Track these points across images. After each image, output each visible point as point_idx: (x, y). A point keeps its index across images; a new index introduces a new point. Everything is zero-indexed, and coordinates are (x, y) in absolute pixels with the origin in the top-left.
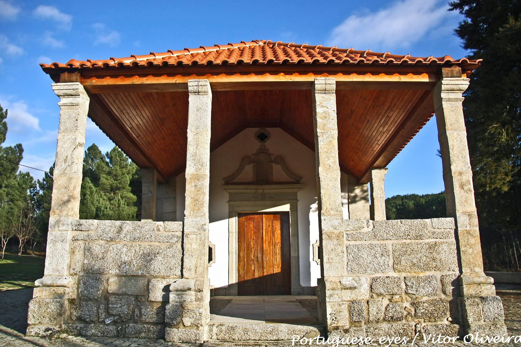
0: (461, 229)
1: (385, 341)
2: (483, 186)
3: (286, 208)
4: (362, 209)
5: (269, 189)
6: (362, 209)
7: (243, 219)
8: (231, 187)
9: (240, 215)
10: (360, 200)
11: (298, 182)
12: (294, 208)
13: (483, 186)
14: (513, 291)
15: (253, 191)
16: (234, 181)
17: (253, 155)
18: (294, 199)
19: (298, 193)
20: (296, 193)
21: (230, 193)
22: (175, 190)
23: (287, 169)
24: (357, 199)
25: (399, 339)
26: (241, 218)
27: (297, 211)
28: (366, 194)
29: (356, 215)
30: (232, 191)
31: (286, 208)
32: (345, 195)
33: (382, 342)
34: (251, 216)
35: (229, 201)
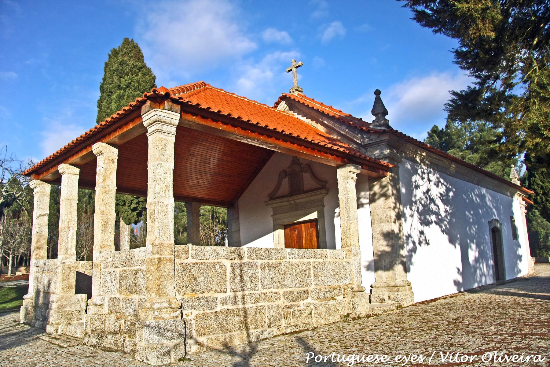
0: (168, 164)
1: (401, 359)
2: (144, 75)
3: (314, 215)
4: (383, 206)
5: (301, 199)
6: (383, 206)
7: (288, 230)
8: (273, 202)
9: (285, 227)
10: (379, 198)
11: (323, 187)
12: (321, 214)
13: (144, 75)
14: (523, 292)
15: (287, 203)
16: (276, 196)
17: (288, 168)
18: (320, 206)
19: (324, 199)
20: (323, 199)
21: (273, 208)
22: (238, 212)
23: (314, 176)
24: (377, 197)
25: (401, 357)
26: (286, 230)
27: (324, 217)
28: (386, 189)
29: (378, 214)
30: (274, 206)
31: (314, 215)
32: (365, 194)
33: (398, 360)
34: (294, 227)
35: (273, 215)
